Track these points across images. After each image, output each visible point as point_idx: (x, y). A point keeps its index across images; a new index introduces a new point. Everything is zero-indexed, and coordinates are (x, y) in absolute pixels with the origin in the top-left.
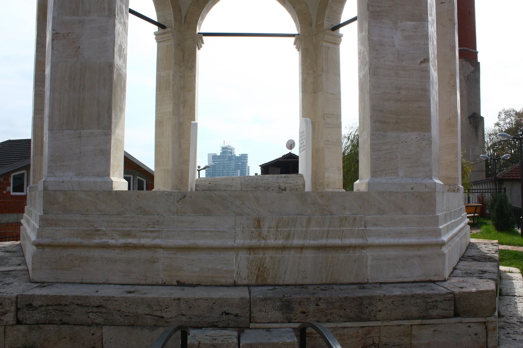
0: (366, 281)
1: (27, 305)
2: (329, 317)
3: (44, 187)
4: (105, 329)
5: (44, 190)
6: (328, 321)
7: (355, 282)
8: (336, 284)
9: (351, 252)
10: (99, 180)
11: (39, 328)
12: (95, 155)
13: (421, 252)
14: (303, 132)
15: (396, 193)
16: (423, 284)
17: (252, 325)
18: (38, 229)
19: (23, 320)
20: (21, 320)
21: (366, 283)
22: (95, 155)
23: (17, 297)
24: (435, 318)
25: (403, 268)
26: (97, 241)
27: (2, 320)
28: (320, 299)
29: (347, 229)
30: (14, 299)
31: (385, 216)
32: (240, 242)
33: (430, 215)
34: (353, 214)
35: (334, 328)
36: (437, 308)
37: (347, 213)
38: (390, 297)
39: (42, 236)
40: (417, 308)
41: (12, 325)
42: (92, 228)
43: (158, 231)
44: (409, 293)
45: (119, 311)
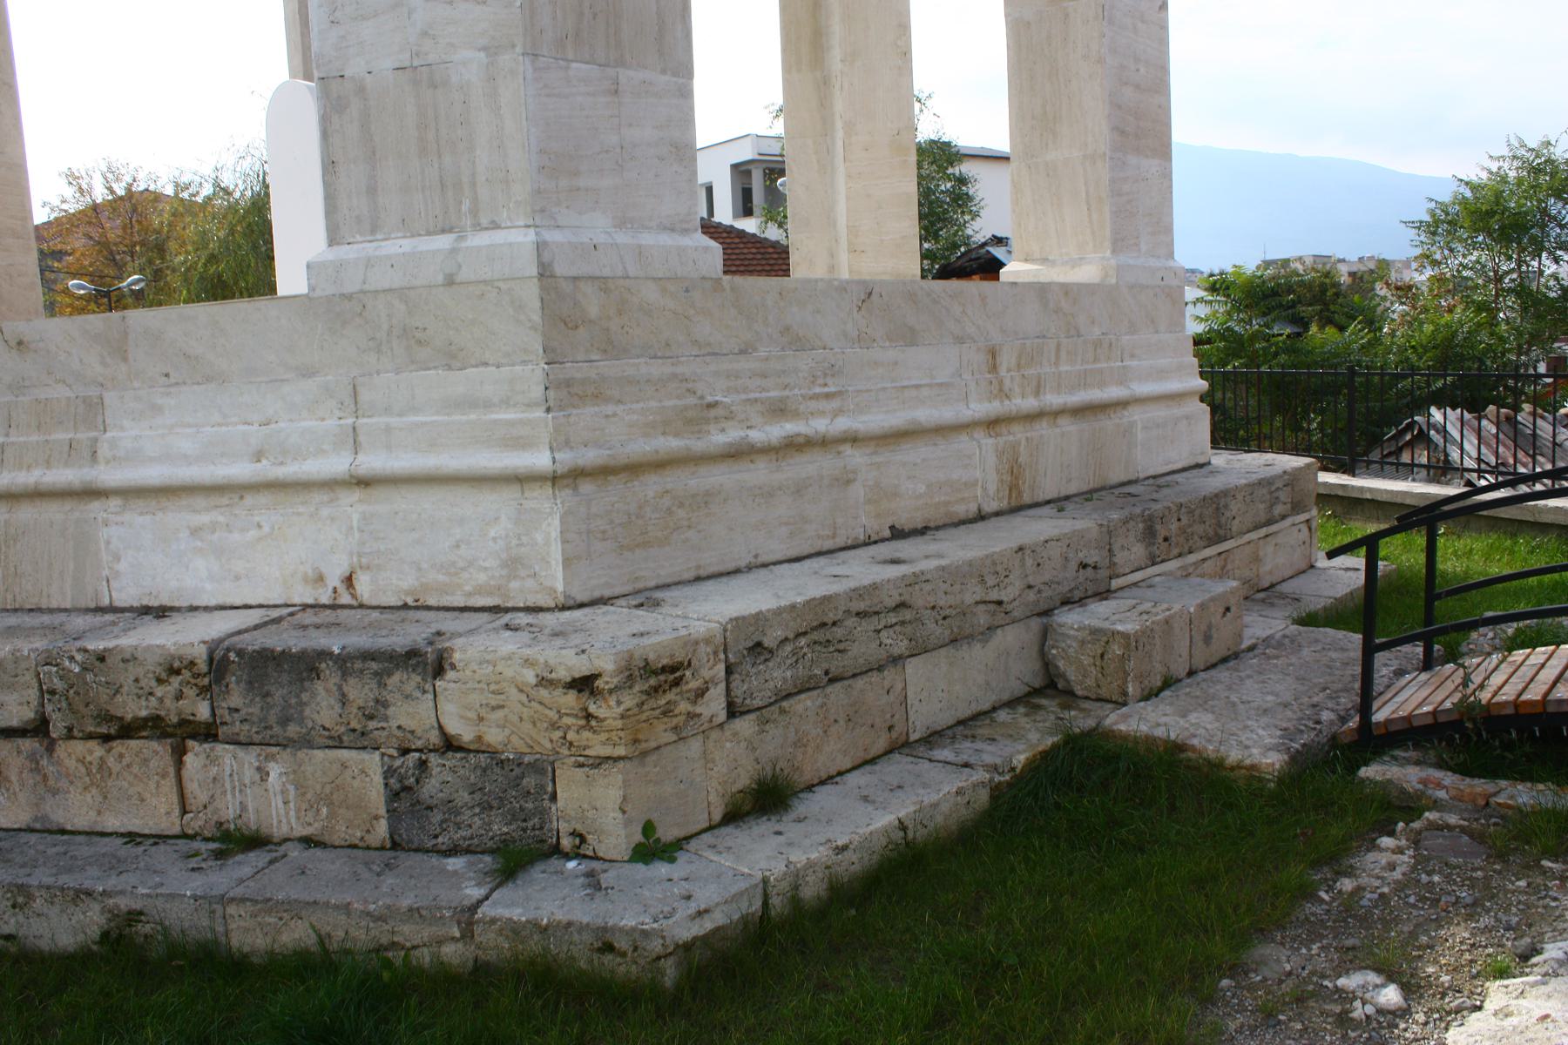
1: (750, 649)
4: (912, 666)
5: (541, 275)
11: (783, 711)
12: (661, 159)
17: (1115, 583)
22: (661, 159)
26: (722, 437)
27: (699, 715)
32: (980, 408)
39: (567, 443)
42: (691, 400)
43: (840, 393)
45: (933, 608)
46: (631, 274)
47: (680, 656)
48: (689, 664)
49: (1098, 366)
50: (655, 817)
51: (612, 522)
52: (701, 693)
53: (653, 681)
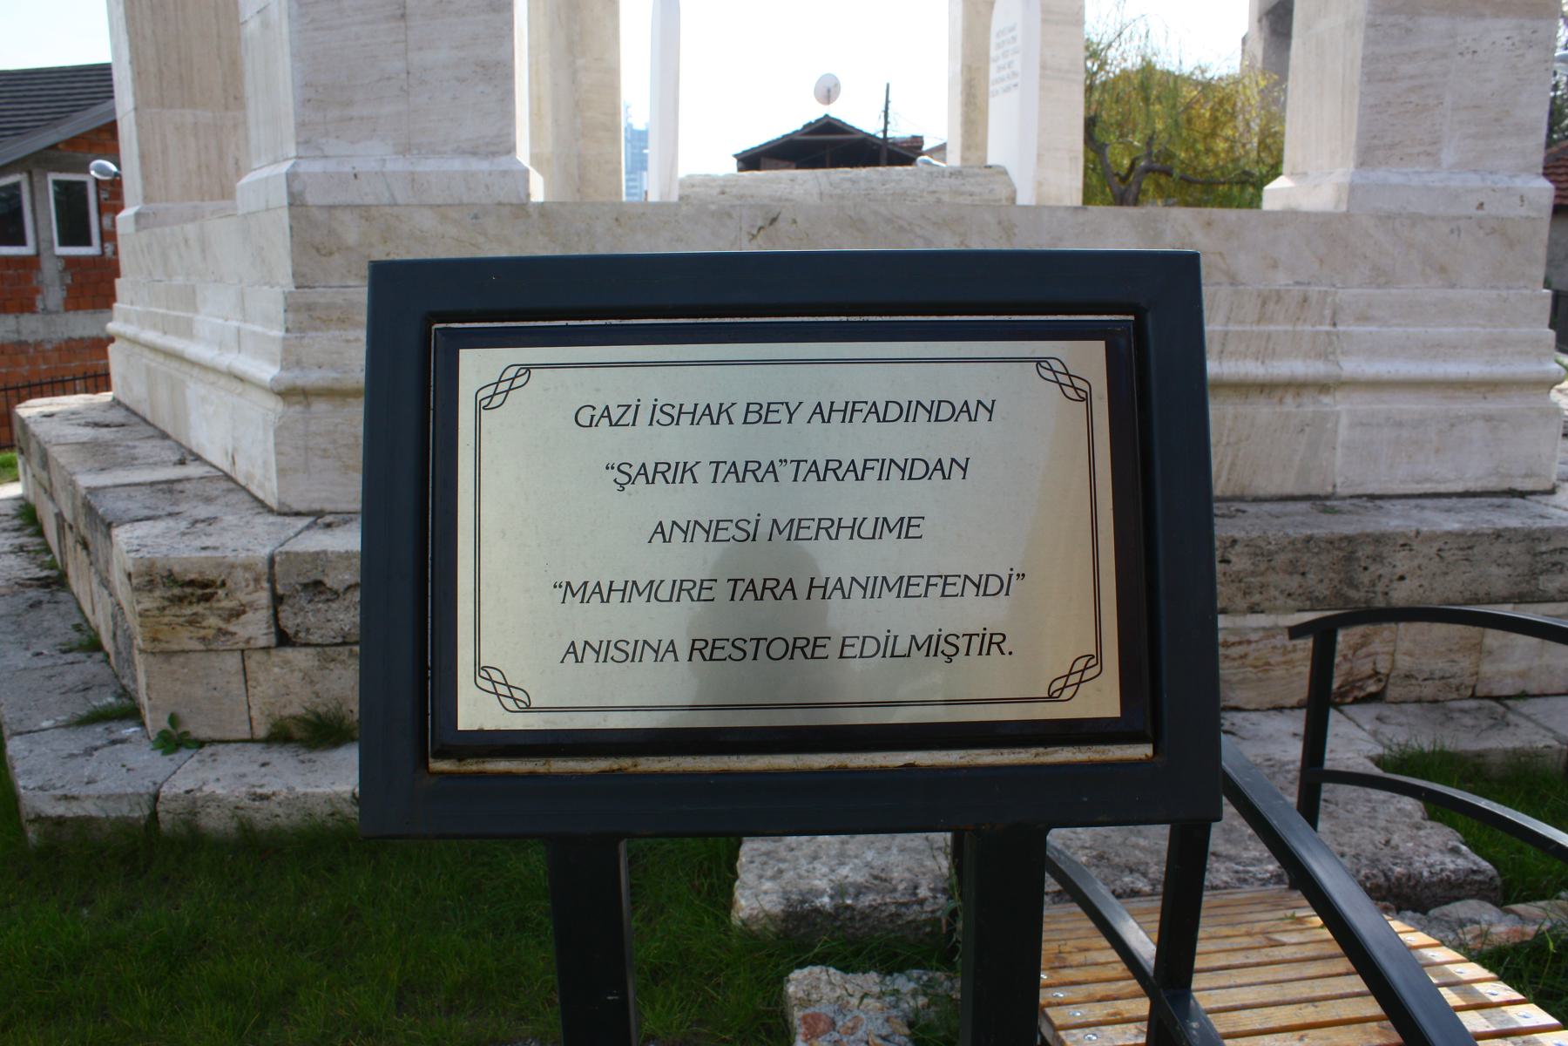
0: (1330, 489)
1: (305, 586)
2: (1257, 598)
3: (291, 194)
5: (291, 205)
6: (1253, 609)
7: (1297, 492)
8: (1241, 499)
9: (1289, 399)
10: (480, 165)
12: (461, 80)
13: (1493, 405)
14: (1012, 29)
15: (1432, 218)
16: (1496, 501)
18: (284, 339)
19: (297, 633)
20: (291, 631)
21: (1327, 498)
23: (271, 561)
24: (1552, 600)
25: (1437, 451)
27: (233, 634)
28: (1234, 542)
29: (1280, 328)
30: (263, 568)
31: (1393, 291)
33: (1525, 292)
34: (1297, 283)
35: (1270, 629)
36: (1561, 571)
37: (1281, 279)
38: (1432, 537)
39: (298, 363)
40: (1507, 570)
41: (266, 649)
44: (1486, 527)
46: (400, 201)
47: (211, 574)
48: (223, 584)
49: (1263, 328)
50: (183, 712)
51: (334, 442)
52: (237, 614)
53: (177, 591)
